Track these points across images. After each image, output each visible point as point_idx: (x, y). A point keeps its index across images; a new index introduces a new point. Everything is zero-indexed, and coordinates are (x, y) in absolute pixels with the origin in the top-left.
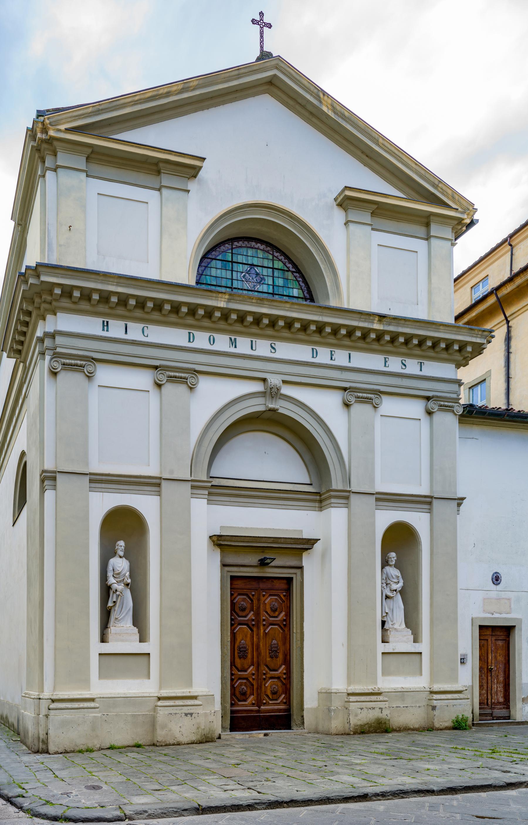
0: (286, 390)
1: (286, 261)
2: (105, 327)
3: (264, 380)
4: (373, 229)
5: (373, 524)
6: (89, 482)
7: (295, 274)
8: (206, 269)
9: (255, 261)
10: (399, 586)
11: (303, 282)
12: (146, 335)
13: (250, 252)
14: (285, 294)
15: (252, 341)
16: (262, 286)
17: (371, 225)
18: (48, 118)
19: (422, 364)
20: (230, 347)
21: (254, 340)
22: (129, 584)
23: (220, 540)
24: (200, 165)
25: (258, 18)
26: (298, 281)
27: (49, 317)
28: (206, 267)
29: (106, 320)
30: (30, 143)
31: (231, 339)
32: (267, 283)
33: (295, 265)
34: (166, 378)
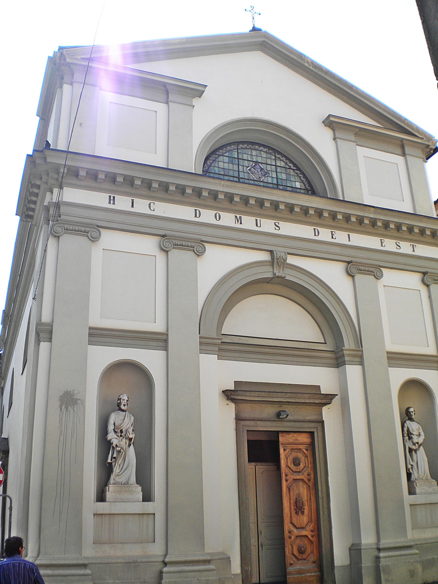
0: (291, 260)
1: (287, 161)
2: (112, 202)
3: (271, 252)
4: (357, 145)
5: (387, 380)
7: (296, 171)
8: (215, 162)
9: (259, 160)
10: (421, 440)
11: (304, 178)
12: (152, 209)
13: (254, 153)
14: (288, 185)
15: (256, 220)
16: (266, 178)
17: (356, 142)
18: (66, 51)
19: (414, 246)
20: (235, 223)
21: (258, 219)
22: (132, 438)
23: (234, 395)
24: (203, 90)
26: (300, 177)
27: (56, 191)
28: (214, 161)
29: (112, 195)
31: (236, 217)
32: (271, 176)
33: (295, 165)
34: (173, 246)
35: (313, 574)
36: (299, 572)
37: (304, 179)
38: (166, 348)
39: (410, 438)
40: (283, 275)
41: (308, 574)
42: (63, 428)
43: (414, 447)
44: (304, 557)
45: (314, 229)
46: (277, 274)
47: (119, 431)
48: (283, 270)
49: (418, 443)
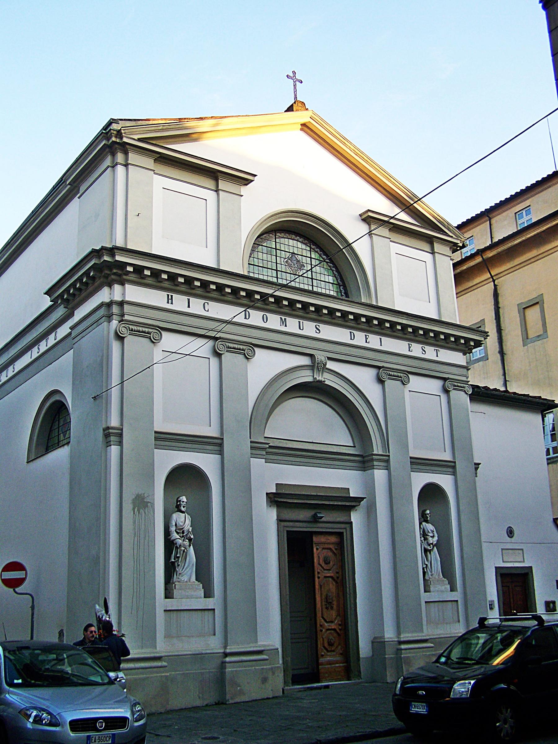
0: (330, 365)
3: (311, 356)
6: (155, 440)
11: (336, 271)
25: (291, 75)
26: (333, 271)
29: (170, 294)
30: (103, 141)
35: (341, 665)
36: (330, 663)
37: (336, 273)
38: (221, 453)
39: (425, 539)
40: (323, 380)
41: (337, 665)
42: (137, 530)
43: (429, 548)
44: (333, 649)
45: (351, 332)
46: (318, 379)
47: (180, 531)
48: (322, 374)
49: (432, 544)
